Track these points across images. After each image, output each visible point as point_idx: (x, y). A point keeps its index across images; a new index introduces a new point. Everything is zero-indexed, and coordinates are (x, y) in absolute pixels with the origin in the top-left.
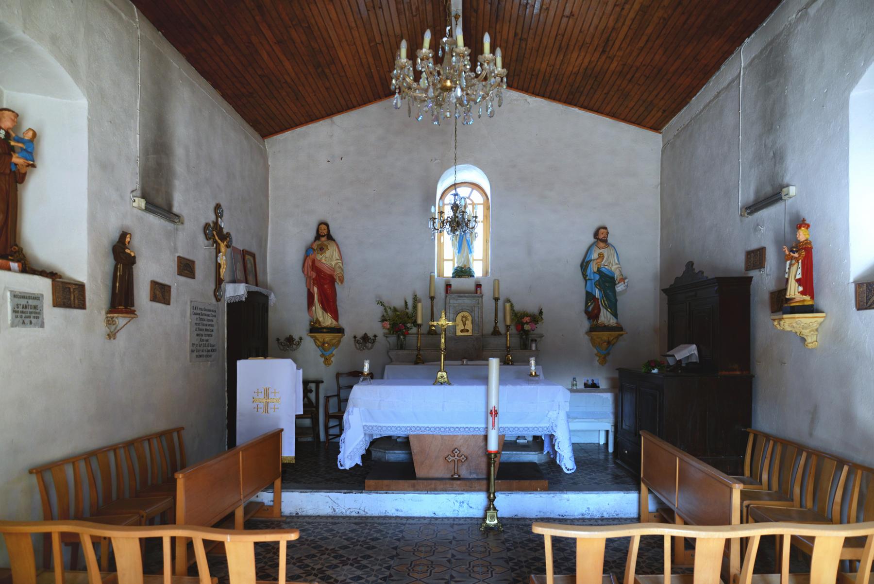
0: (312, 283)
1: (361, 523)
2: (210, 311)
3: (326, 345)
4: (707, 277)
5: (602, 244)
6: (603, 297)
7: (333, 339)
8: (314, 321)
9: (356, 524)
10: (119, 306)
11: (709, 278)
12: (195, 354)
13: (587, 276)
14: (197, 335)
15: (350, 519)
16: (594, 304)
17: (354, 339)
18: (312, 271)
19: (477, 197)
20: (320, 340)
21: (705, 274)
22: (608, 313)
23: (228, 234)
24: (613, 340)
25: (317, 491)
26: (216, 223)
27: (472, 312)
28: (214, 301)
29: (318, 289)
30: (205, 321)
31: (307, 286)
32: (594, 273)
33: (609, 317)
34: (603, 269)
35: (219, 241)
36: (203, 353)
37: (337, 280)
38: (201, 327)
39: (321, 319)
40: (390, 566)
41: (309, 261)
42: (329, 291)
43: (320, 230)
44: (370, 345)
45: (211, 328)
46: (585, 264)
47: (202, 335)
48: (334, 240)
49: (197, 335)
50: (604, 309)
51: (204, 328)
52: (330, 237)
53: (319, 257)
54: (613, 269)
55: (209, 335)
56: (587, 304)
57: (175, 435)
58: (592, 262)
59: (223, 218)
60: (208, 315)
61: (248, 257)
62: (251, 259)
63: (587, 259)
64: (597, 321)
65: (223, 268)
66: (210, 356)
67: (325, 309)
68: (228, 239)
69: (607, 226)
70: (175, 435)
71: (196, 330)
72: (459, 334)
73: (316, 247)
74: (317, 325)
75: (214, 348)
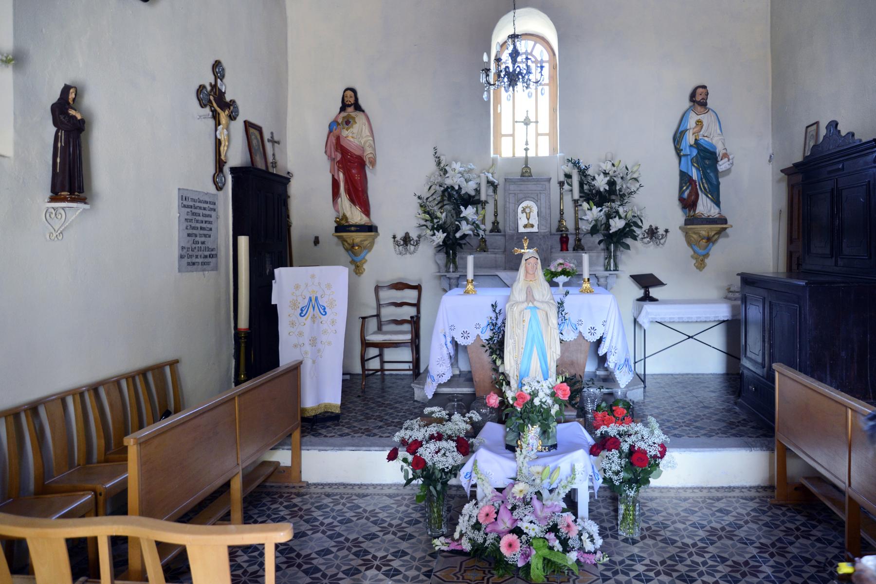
0: (336, 167)
1: (398, 495)
2: (206, 202)
3: (357, 248)
4: (860, 140)
5: (699, 108)
6: (701, 179)
7: (365, 240)
8: (341, 217)
9: (390, 496)
10: (61, 192)
11: (864, 140)
12: (186, 260)
13: (682, 150)
14: (189, 235)
15: (382, 489)
16: (690, 188)
17: (393, 240)
18: (337, 151)
19: (540, 52)
20: (349, 241)
21: (857, 137)
22: (708, 200)
23: (233, 102)
24: (714, 236)
25: (340, 448)
26: (214, 86)
27: (537, 201)
28: (212, 189)
29: (344, 174)
30: (199, 216)
31: (330, 172)
32: (691, 146)
33: (709, 205)
34: (702, 141)
35: (218, 110)
36: (197, 260)
37: (367, 163)
38: (193, 224)
39: (348, 214)
40: (431, 571)
41: (333, 137)
42: (357, 177)
43: (345, 98)
44: (412, 248)
45: (209, 226)
46: (678, 135)
47: (196, 236)
48: (363, 111)
49: (189, 235)
50: (703, 195)
51: (199, 225)
52: (358, 107)
53: (345, 133)
54: (714, 142)
55: (205, 236)
56: (681, 188)
57: (168, 370)
58: (688, 131)
59: (224, 80)
60: (205, 209)
61: (252, 130)
62: (257, 133)
63: (681, 129)
64: (695, 211)
65: (224, 146)
66: (208, 263)
67: (352, 200)
68: (232, 108)
69: (706, 85)
70: (168, 370)
71: (187, 228)
72: (521, 230)
73: (341, 120)
74: (343, 222)
75: (213, 253)
